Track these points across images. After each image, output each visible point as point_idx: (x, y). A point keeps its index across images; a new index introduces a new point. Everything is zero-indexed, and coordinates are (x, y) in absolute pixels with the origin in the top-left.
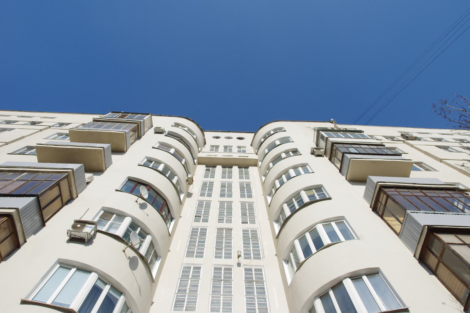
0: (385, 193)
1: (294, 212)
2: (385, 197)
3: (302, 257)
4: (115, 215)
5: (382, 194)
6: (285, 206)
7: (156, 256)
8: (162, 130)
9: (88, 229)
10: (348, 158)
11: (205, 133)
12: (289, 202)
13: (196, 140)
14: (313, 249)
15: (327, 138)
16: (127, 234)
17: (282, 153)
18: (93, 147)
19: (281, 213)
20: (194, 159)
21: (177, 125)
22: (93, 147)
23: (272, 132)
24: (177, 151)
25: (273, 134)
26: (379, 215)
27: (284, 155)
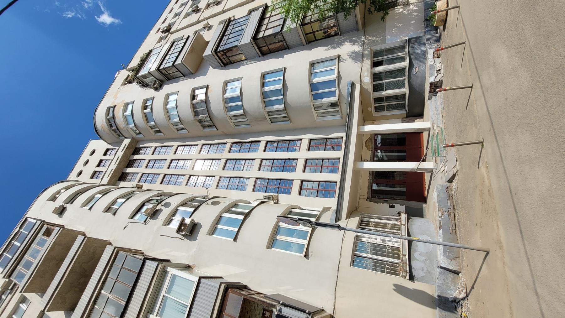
3: (241, 112)
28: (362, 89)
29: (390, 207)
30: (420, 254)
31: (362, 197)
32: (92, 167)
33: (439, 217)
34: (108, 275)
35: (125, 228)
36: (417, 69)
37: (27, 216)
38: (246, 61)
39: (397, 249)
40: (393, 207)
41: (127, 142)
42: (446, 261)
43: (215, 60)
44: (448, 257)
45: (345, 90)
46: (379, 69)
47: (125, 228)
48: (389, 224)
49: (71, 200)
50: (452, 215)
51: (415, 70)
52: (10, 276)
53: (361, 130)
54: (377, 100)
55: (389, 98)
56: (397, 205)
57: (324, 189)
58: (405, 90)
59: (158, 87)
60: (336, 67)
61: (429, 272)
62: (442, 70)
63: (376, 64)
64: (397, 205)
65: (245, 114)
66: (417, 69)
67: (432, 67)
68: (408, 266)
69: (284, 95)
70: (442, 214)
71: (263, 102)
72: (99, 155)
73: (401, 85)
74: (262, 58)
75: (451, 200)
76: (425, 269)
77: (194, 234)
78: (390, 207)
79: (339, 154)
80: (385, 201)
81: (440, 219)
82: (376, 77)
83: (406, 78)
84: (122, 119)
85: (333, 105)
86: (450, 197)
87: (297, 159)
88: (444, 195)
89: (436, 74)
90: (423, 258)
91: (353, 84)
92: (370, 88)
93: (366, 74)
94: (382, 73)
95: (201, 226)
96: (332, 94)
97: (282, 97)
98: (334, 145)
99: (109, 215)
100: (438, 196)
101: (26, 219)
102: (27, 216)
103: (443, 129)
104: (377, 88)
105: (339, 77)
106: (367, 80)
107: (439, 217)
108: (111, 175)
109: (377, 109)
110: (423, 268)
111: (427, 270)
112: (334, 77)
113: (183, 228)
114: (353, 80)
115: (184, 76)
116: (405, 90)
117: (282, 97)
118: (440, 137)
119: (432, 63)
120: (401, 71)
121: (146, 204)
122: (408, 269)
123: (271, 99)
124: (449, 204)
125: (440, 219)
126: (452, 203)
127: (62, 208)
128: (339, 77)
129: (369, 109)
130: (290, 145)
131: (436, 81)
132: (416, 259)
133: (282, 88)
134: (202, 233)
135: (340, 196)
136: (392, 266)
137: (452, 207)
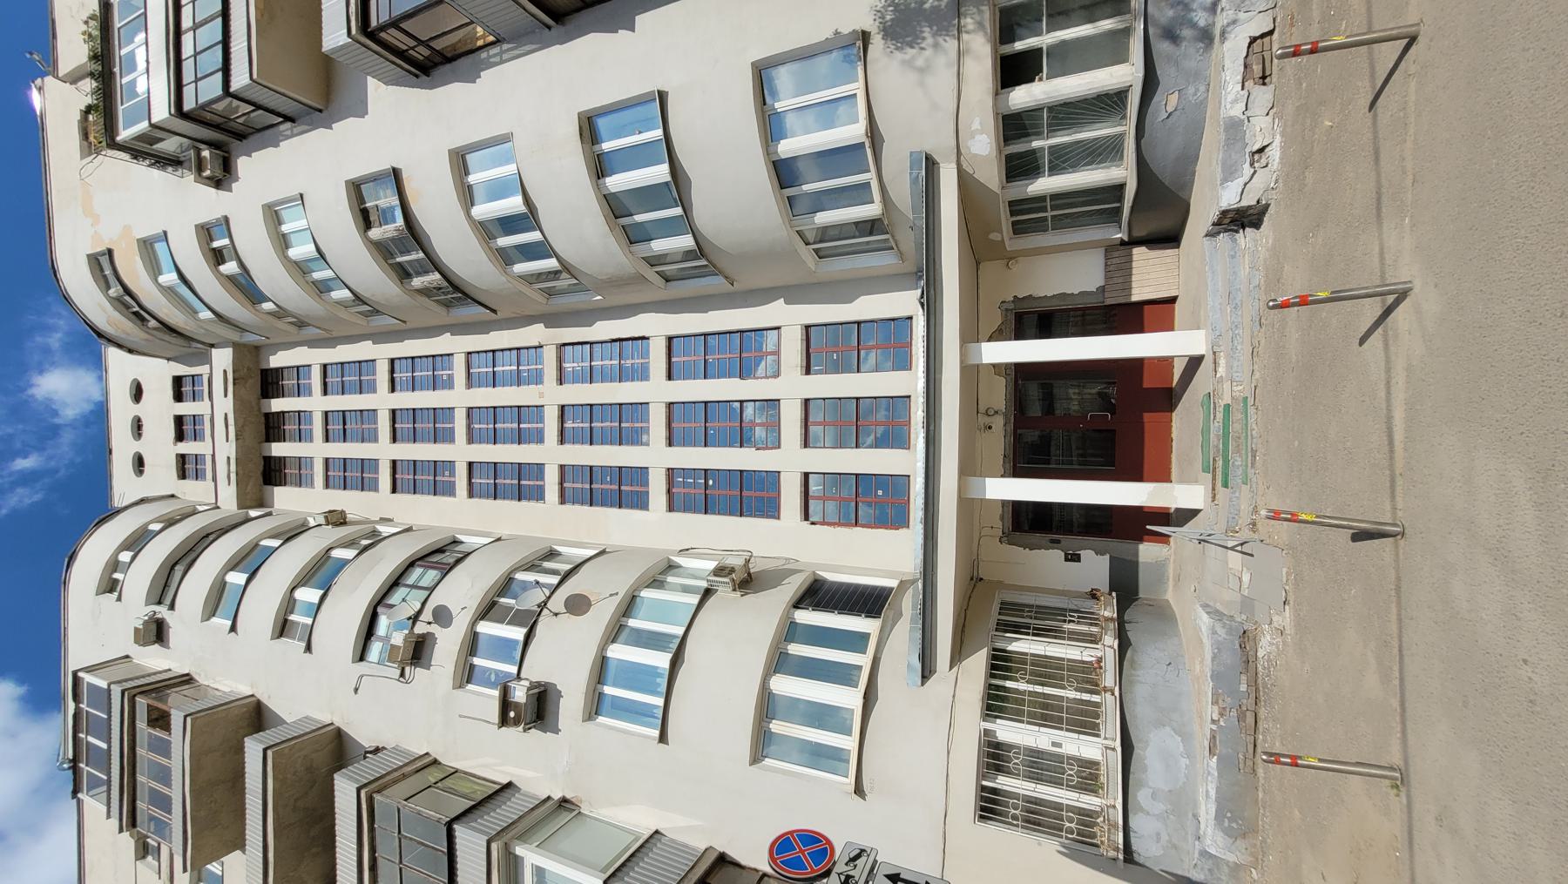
0: (383, 28)
1: (434, 263)
2: (392, 31)
3: (551, 264)
4: (476, 661)
5: (383, 35)
6: (417, 282)
7: (552, 554)
8: (146, 623)
9: (520, 694)
10: (246, 87)
11: (118, 502)
12: (403, 273)
13: (170, 522)
14: (535, 236)
15: (151, 125)
16: (517, 618)
17: (219, 275)
18: (185, 832)
19: (429, 297)
20: (248, 520)
21: (110, 586)
22: (185, 832)
23: (115, 291)
24: (234, 565)
25: (241, 264)
26: (442, 63)
27: (230, 267)
28: (966, 183)
29: (1067, 560)
30: (1154, 796)
31: (986, 531)
32: (161, 447)
33: (1213, 721)
34: (373, 850)
35: (356, 690)
36: (1173, 100)
37: (71, 668)
38: (495, 50)
39: (1093, 764)
40: (1075, 558)
41: (222, 359)
42: (1220, 838)
43: (370, 57)
44: (1228, 832)
45: (904, 192)
46: (1022, 96)
47: (356, 690)
48: (1071, 787)
49: (164, 588)
50: (1250, 719)
51: (1167, 101)
52: (133, 823)
53: (973, 361)
54: (1016, 207)
55: (1061, 198)
56: (1087, 555)
57: (872, 502)
58: (1122, 172)
59: (219, 173)
60: (857, 87)
61: (1175, 847)
62: (1274, 153)
63: (1014, 70)
64: (1087, 555)
65: (566, 267)
66: (1173, 100)
67: (1235, 129)
68: (1121, 835)
69: (684, 201)
70: (1221, 715)
71: (619, 231)
72: (160, 409)
73: (1106, 151)
74: (557, 30)
75: (1252, 671)
76: (1165, 837)
77: (549, 717)
78: (1067, 560)
79: (907, 462)
80: (1053, 541)
81: (1214, 727)
82: (1014, 126)
83: (1129, 128)
84: (163, 300)
85: (870, 226)
86: (1248, 661)
87: (778, 328)
88: (1231, 658)
89: (1247, 170)
90: (1159, 807)
91: (931, 164)
92: (990, 175)
93: (976, 125)
94: (1039, 109)
95: (559, 694)
96: (859, 193)
97: (678, 211)
98: (889, 340)
99: (295, 645)
100: (1214, 658)
101: (77, 681)
102: (71, 668)
103: (1251, 411)
104: (1019, 167)
105: (874, 133)
106: (983, 144)
107: (1213, 721)
108: (233, 476)
109: (1019, 229)
110: (1158, 834)
111: (1169, 841)
112: (852, 131)
113: (512, 714)
114: (928, 146)
115: (288, 119)
116: (1122, 172)
117: (678, 211)
118: (1237, 427)
119: (1237, 111)
120: (1110, 103)
121: (380, 609)
122: (1121, 841)
123: (639, 218)
124: (1243, 688)
125: (1214, 727)
126: (1254, 682)
127: (154, 627)
128: (874, 133)
129: (995, 236)
130: (744, 354)
131: (1244, 203)
132: (1142, 810)
133: (668, 178)
134: (570, 705)
135: (929, 589)
136: (1080, 823)
137: (1253, 695)
